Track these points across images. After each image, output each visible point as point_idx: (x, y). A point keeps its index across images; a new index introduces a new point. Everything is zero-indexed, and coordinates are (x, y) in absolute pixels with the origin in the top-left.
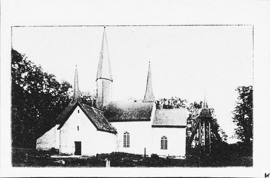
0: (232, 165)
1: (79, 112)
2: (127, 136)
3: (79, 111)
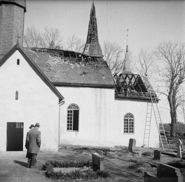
0: (21, 53)
1: (18, 63)
2: (129, 120)
3: (18, 61)
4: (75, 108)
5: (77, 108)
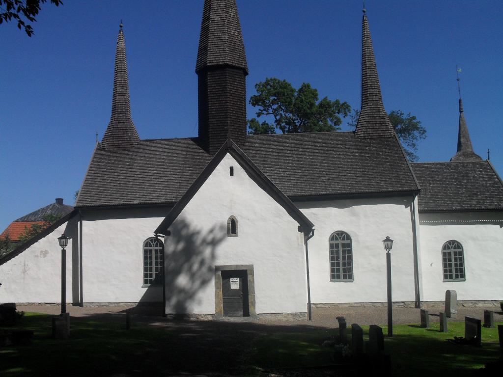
1: (232, 174)
2: (340, 246)
3: (232, 169)
4: (343, 239)
5: (459, 248)
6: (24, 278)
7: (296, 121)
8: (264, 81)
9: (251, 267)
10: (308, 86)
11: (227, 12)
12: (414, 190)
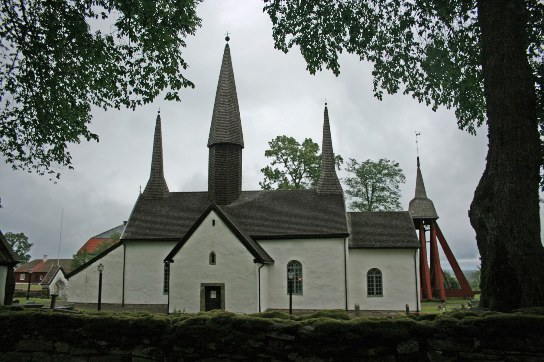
1: (214, 224)
3: (214, 221)
6: (86, 286)
7: (281, 178)
8: (275, 138)
9: (223, 285)
10: (310, 140)
11: (229, 105)
12: (345, 234)
